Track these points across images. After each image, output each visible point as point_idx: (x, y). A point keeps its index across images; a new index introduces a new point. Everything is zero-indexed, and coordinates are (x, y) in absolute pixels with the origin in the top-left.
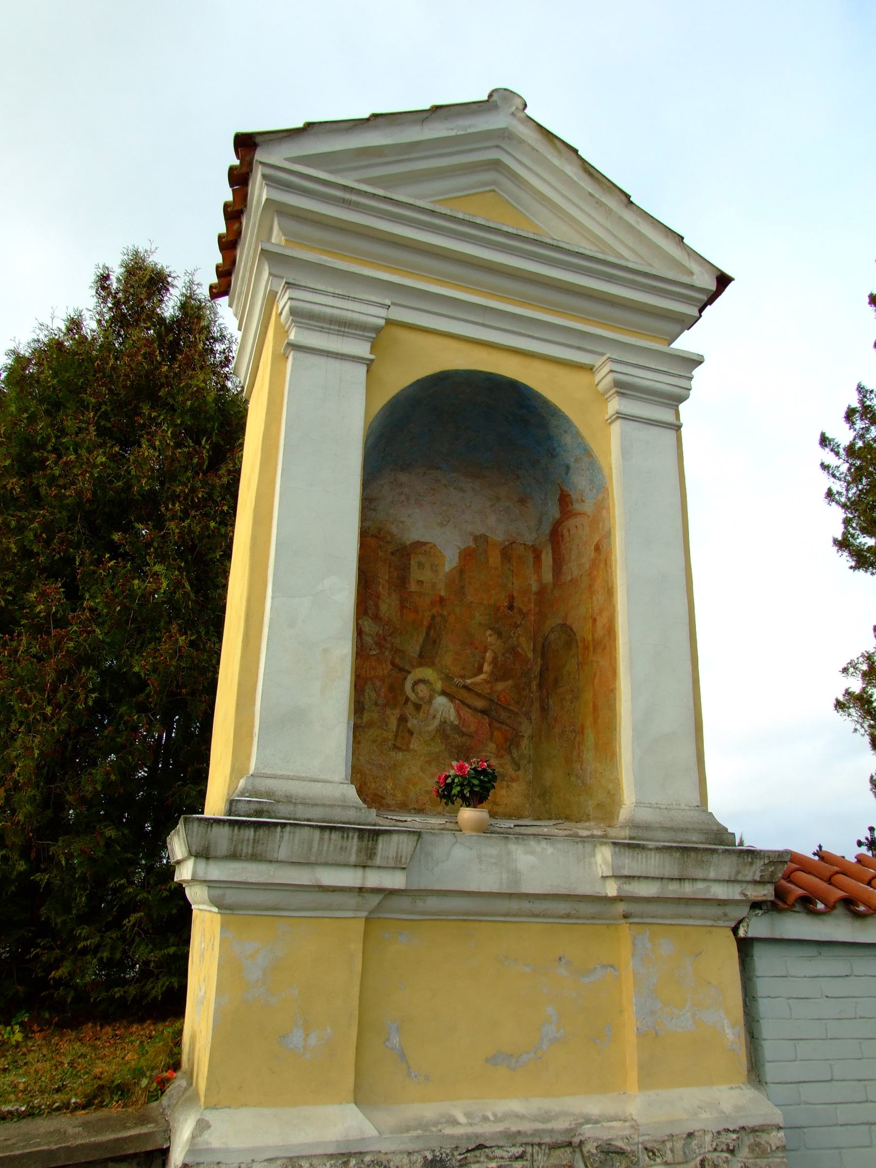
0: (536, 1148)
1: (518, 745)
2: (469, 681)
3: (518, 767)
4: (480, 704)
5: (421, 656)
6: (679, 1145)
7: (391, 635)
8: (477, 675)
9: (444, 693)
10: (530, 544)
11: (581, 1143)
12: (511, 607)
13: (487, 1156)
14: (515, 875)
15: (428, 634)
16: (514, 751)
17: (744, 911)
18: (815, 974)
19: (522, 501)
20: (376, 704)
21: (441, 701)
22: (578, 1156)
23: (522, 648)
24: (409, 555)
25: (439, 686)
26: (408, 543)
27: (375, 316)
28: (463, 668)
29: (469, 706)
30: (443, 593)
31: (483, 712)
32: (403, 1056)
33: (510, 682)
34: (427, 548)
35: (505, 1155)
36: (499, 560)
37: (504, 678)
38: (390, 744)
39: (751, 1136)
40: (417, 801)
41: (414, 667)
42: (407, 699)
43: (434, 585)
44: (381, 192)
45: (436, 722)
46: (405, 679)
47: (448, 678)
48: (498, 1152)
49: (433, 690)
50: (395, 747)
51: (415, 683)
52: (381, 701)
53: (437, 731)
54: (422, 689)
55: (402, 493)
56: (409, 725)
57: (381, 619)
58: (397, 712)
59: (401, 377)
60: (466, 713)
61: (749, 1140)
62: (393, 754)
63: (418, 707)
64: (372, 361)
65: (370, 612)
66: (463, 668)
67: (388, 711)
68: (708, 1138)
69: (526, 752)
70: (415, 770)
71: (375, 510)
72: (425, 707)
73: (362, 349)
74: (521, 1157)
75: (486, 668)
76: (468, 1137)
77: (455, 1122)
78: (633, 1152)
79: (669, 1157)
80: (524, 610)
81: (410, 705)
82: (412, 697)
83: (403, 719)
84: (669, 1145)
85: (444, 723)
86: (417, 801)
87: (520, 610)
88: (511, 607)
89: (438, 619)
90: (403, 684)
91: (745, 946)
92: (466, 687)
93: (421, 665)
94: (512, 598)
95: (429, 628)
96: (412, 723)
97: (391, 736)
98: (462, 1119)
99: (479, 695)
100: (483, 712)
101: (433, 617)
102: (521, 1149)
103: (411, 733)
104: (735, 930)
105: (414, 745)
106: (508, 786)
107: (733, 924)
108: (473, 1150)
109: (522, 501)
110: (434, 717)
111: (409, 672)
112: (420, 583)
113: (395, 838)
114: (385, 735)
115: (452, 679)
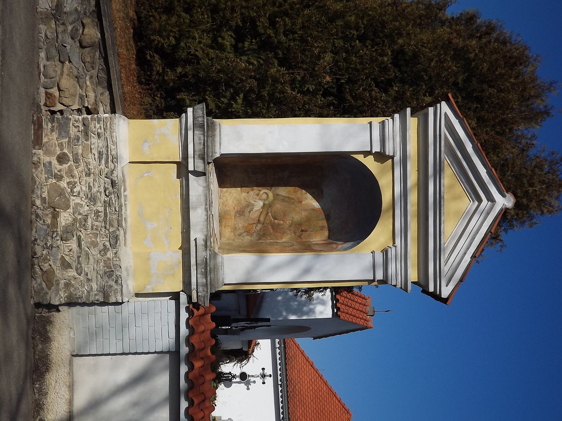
1: (248, 235)
4: (262, 219)
9: (264, 205)
14: (195, 208)
15: (286, 197)
16: (246, 233)
21: (261, 203)
22: (115, 229)
29: (260, 215)
30: (303, 202)
31: (259, 220)
32: (142, 176)
36: (321, 225)
41: (273, 192)
44: (443, 149)
45: (253, 202)
48: (117, 203)
54: (264, 196)
60: (257, 214)
69: (245, 238)
70: (235, 195)
72: (258, 198)
75: (276, 221)
76: (121, 194)
77: (125, 191)
79: (115, 259)
81: (258, 192)
82: (261, 192)
85: (253, 205)
87: (302, 235)
88: (302, 231)
89: (293, 201)
91: (175, 296)
93: (274, 195)
94: (306, 231)
95: (289, 198)
98: (125, 193)
99: (265, 218)
100: (259, 220)
101: (293, 199)
103: (248, 193)
113: (203, 165)
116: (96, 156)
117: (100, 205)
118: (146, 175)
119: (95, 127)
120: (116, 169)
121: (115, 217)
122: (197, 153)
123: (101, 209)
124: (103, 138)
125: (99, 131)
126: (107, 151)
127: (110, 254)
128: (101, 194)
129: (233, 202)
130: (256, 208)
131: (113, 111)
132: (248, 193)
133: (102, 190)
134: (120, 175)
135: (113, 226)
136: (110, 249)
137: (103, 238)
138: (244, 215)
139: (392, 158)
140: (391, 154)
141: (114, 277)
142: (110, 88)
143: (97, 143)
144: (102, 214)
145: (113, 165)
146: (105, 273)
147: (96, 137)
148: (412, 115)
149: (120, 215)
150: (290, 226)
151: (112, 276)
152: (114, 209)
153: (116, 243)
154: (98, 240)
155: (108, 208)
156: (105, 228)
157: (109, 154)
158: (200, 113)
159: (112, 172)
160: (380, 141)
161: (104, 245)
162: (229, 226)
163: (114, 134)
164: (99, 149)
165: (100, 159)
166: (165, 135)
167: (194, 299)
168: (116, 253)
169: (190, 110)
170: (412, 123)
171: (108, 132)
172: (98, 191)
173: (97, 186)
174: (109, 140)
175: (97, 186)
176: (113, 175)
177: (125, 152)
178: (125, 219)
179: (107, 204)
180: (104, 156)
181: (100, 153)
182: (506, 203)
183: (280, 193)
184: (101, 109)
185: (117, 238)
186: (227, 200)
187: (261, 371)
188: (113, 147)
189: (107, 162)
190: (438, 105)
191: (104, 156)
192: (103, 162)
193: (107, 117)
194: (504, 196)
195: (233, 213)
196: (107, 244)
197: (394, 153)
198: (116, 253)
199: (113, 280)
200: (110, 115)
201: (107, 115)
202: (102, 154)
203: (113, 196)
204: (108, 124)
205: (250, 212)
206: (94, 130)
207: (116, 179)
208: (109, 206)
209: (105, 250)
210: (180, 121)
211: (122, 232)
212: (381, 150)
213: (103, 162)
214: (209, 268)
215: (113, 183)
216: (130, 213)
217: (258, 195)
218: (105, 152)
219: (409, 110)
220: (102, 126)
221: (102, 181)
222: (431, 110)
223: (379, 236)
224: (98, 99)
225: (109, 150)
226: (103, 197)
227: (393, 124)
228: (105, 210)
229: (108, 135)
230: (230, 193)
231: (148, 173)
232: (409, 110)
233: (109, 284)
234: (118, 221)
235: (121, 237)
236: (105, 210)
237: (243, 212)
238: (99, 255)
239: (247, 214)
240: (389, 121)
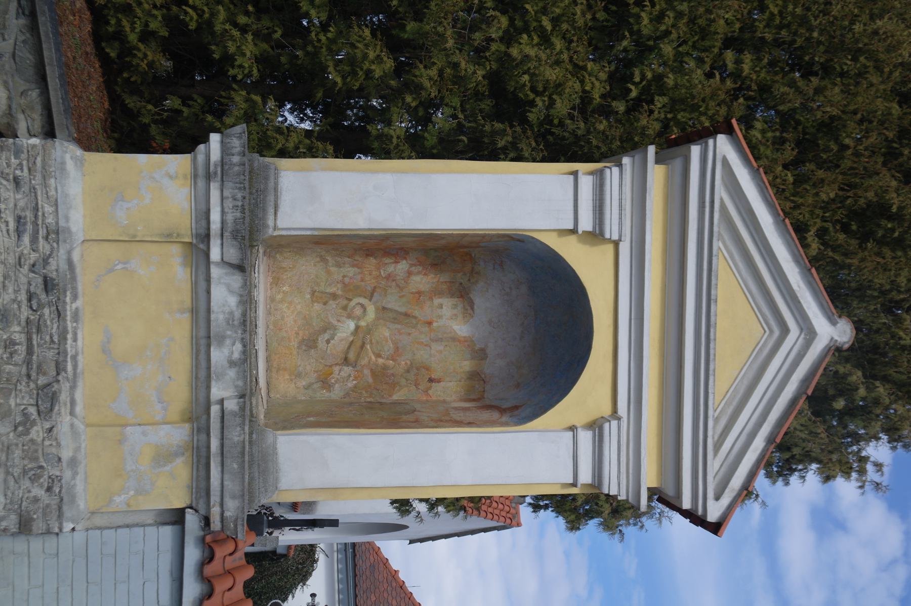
0: (56, 351)
1: (323, 388)
2: (368, 347)
3: (307, 387)
4: (352, 356)
5: (384, 308)
6: (54, 450)
7: (398, 286)
8: (374, 353)
9: (357, 328)
10: (485, 396)
11: (58, 381)
12: (431, 380)
13: (53, 319)
15: (401, 313)
17: (202, 511)
18: (160, 575)
19: (518, 386)
20: (344, 276)
21: (352, 325)
23: (399, 391)
24: (462, 296)
25: (363, 323)
26: (471, 296)
27: (611, 230)
28: (377, 342)
29: (349, 348)
30: (435, 324)
31: (346, 359)
32: (111, 271)
33: (370, 380)
34: (470, 311)
35: (54, 330)
37: (374, 373)
38: (316, 288)
39: (56, 507)
40: (276, 310)
42: (350, 300)
43: (440, 317)
45: (335, 323)
46: (365, 297)
47: (369, 330)
48: (55, 326)
49: (359, 319)
50: (313, 293)
51: (362, 306)
52: (347, 280)
53: (329, 323)
54: (358, 311)
55: (511, 288)
56: (331, 302)
57: (409, 277)
58: (340, 292)
59: (573, 253)
60: (343, 346)
61: (54, 502)
62: (309, 290)
63: (345, 308)
64: (577, 232)
65: (413, 268)
66: (377, 342)
67: (339, 286)
68: (58, 473)
71: (494, 268)
73: (586, 224)
74: (52, 341)
75: (380, 361)
78: (51, 417)
79: (47, 443)
80: (430, 392)
81: (345, 302)
82: (353, 303)
83: (334, 296)
84: (54, 443)
86: (276, 310)
87: (430, 388)
88: (431, 380)
89: (414, 321)
90: (360, 296)
92: (363, 346)
93: (377, 309)
96: (332, 304)
97: (322, 288)
100: (346, 359)
102: (56, 340)
103: (325, 304)
104: (191, 508)
105: (317, 307)
106: (291, 380)
107: (194, 505)
108: (57, 309)
109: (518, 386)
110: (339, 321)
111: (370, 300)
112: (441, 306)
114: (322, 284)
115: (369, 334)
116: (12, 225)
117: (17, 329)
118: (119, 267)
119: (8, 165)
120: (54, 254)
121: (51, 354)
122: (230, 226)
123: (19, 337)
124: (25, 188)
125: (18, 172)
126: (36, 216)
127: (37, 433)
128: (20, 307)
129: (295, 321)
130: (340, 335)
131: (50, 133)
132: (325, 304)
133: (23, 297)
134: (63, 266)
135: (44, 374)
136: (38, 421)
137: (23, 397)
138: (316, 347)
139: (616, 244)
140: (615, 237)
141: (44, 480)
142: (42, 79)
143: (12, 200)
144: (22, 349)
145: (48, 247)
146: (25, 472)
147: (11, 186)
148: (657, 162)
149: (62, 353)
150: (408, 371)
151: (40, 477)
152: (48, 338)
153: (51, 410)
154: (12, 402)
155: (34, 336)
156: (29, 376)
157: (40, 222)
158: (237, 144)
159: (46, 262)
160: (594, 210)
161: (25, 414)
162: (285, 370)
163: (52, 181)
164: (18, 212)
165: (19, 233)
166: (160, 185)
167: (216, 525)
168: (50, 430)
169: (215, 138)
170: (656, 174)
171: (39, 176)
172: (14, 301)
173: (11, 290)
174: (39, 193)
175: (11, 290)
176: (48, 268)
177: (77, 220)
178: (74, 358)
179: (33, 327)
180: (29, 227)
181: (19, 219)
182: (836, 338)
183: (389, 306)
184: (22, 126)
185: (54, 398)
186: (283, 318)
187: (309, 600)
188: (48, 209)
189: (34, 240)
190: (711, 142)
191: (29, 227)
192: (26, 239)
193: (34, 146)
194: (833, 323)
195: (294, 343)
196: (32, 410)
197: (620, 236)
198: (50, 430)
199: (41, 486)
200: (43, 142)
201: (35, 141)
202: (25, 224)
203: (46, 311)
204: (39, 159)
205: (328, 342)
206: (7, 171)
207: (54, 275)
208: (39, 330)
209: (26, 423)
210: (194, 160)
211: (65, 387)
212: (594, 227)
213: (26, 239)
214: (256, 463)
215: (48, 285)
216: (85, 342)
217: (345, 308)
218: (29, 215)
219: (652, 149)
220: (25, 163)
221: (23, 280)
222: (695, 150)
223: (590, 392)
224: (14, 106)
225: (40, 214)
226: (25, 313)
227: (619, 177)
228: (29, 340)
229: (37, 181)
230: (290, 303)
231: (125, 263)
232: (652, 149)
233: (32, 494)
234: (57, 364)
235: (64, 396)
236: (29, 340)
237: (315, 341)
238: (12, 434)
239: (321, 344)
240: (612, 174)
